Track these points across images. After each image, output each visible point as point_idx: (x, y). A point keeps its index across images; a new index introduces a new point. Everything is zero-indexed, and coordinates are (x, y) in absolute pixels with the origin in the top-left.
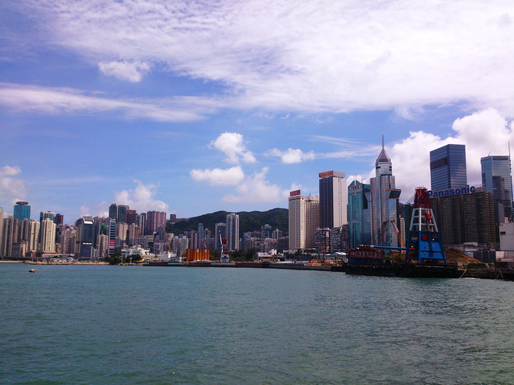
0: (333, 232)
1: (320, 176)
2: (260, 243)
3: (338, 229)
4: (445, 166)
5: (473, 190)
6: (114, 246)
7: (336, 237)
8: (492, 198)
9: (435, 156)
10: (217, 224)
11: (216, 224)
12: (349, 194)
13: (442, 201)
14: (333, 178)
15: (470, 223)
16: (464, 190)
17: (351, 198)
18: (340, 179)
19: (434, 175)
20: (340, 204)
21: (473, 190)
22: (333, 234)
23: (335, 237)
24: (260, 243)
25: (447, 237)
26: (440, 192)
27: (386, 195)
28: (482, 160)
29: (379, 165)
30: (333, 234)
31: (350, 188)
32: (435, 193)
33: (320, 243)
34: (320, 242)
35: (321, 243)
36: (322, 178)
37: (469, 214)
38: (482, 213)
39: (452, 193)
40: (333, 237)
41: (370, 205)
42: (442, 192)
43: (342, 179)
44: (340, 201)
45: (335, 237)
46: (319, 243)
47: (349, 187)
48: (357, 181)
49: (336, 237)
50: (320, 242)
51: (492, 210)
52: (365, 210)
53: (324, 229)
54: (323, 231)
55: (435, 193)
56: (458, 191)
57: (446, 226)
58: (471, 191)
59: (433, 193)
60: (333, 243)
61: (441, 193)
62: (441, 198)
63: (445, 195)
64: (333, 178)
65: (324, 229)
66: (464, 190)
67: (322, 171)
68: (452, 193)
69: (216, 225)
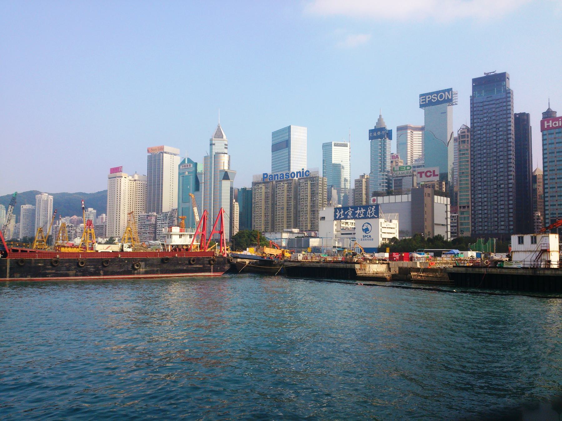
0: (160, 217)
1: (148, 151)
2: (72, 230)
3: (166, 214)
4: (286, 149)
5: (307, 175)
6: (455, 175)
7: (163, 224)
8: (325, 183)
9: (276, 138)
10: (24, 206)
11: (22, 206)
12: (179, 174)
13: (277, 185)
14: (164, 154)
15: (302, 210)
16: (276, 176)
17: (181, 178)
18: (172, 156)
19: (274, 158)
20: (172, 186)
21: (307, 175)
22: (160, 219)
23: (162, 224)
24: (72, 230)
25: (280, 224)
26: (275, 175)
27: (220, 176)
28: (330, 145)
29: (213, 142)
30: (160, 219)
31: (181, 167)
32: (282, 175)
33: (144, 231)
34: (144, 230)
35: (145, 231)
36: (150, 154)
37: (302, 200)
38: (315, 199)
39: (287, 177)
40: (160, 224)
41: (202, 187)
42: (277, 175)
43: (174, 156)
44: (172, 182)
45: (162, 224)
46: (142, 230)
47: (179, 166)
48: (189, 159)
49: (163, 224)
50: (144, 230)
51: (325, 196)
52: (197, 193)
53: (150, 214)
54: (148, 216)
55: (282, 175)
56: (293, 175)
57: (279, 212)
58: (306, 175)
59: (269, 175)
60: (160, 230)
61: (299, 174)
62: (277, 182)
63: (280, 179)
64: (164, 154)
65: (150, 214)
66: (276, 176)
67: (151, 146)
68: (287, 177)
69: (22, 208)
